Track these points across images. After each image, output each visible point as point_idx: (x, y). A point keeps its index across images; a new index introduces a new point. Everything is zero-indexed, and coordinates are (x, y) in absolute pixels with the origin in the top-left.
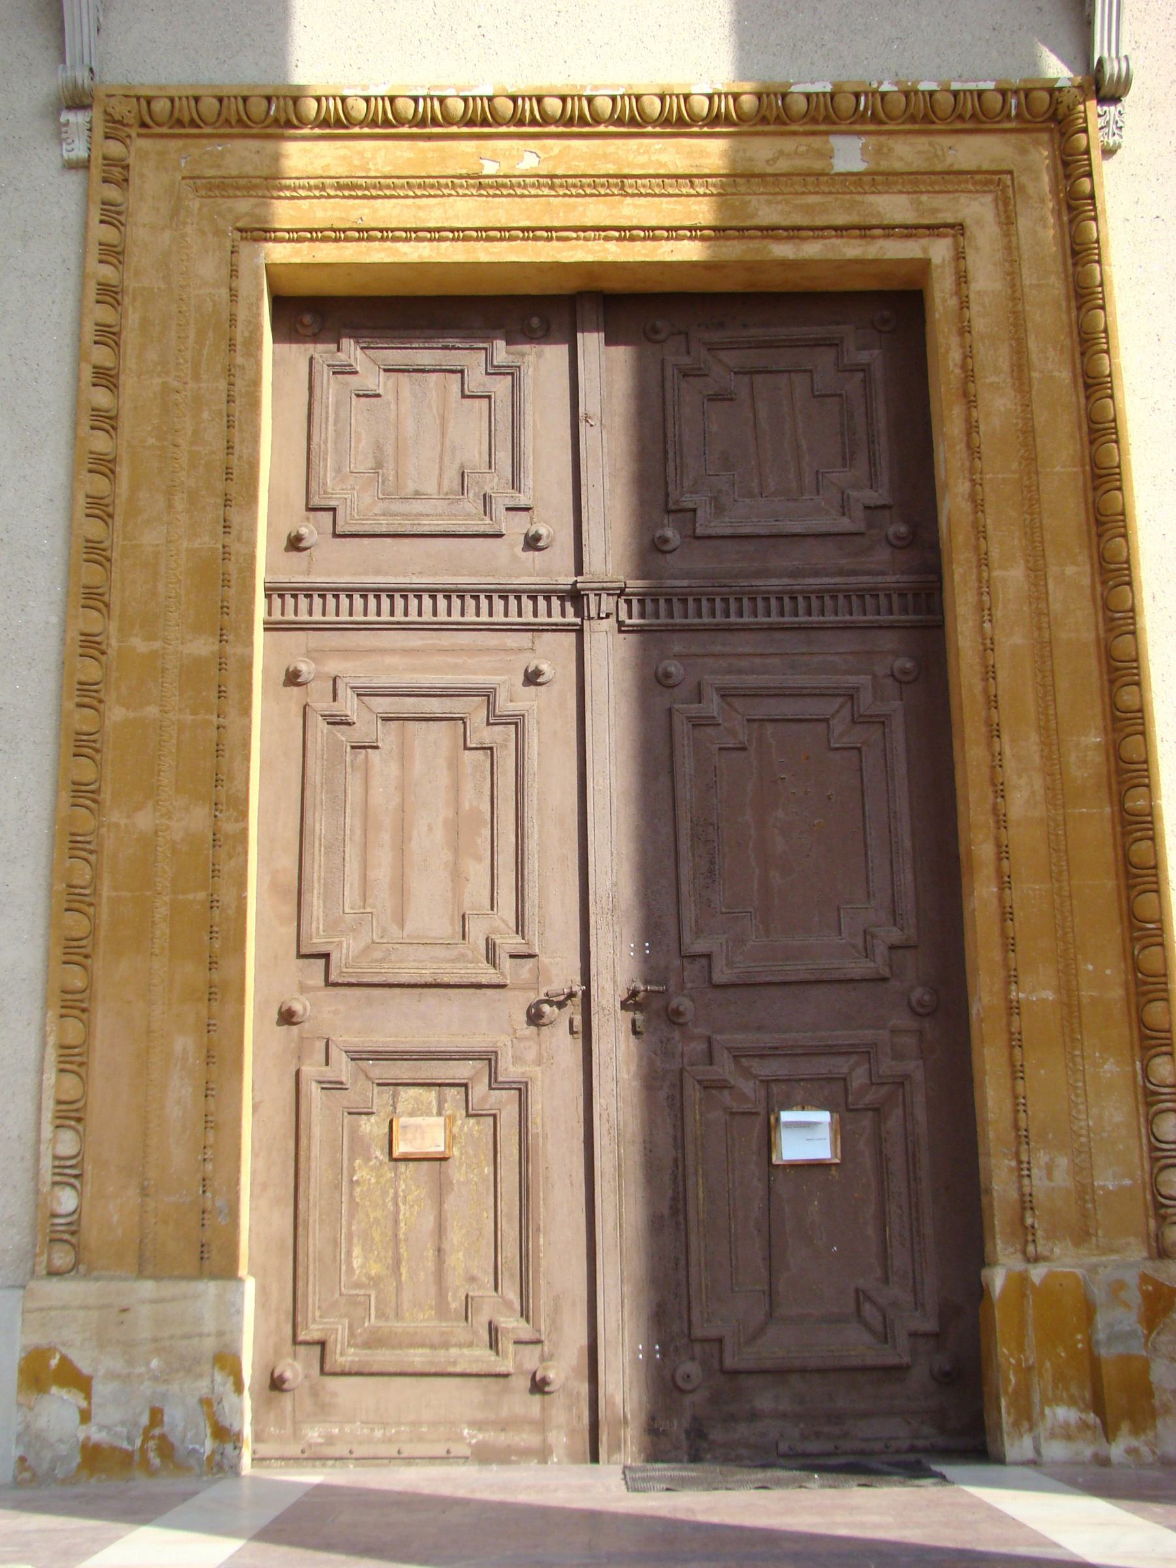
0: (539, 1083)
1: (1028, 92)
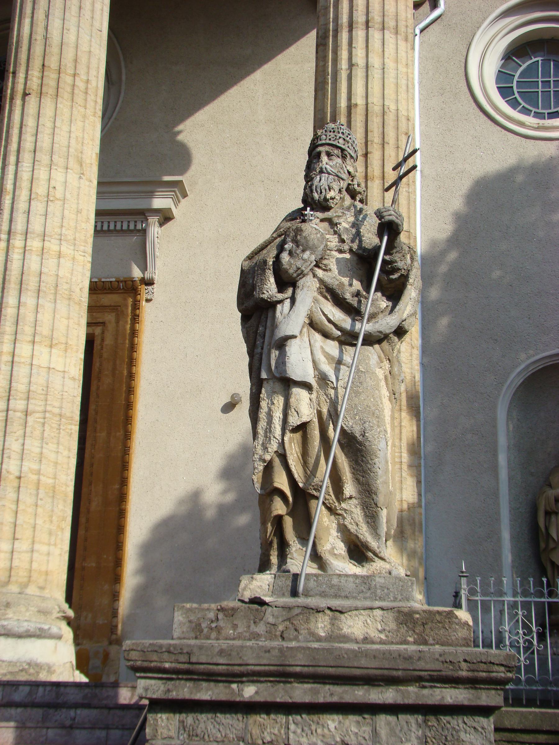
0: (409, 48)
1: (125, 282)
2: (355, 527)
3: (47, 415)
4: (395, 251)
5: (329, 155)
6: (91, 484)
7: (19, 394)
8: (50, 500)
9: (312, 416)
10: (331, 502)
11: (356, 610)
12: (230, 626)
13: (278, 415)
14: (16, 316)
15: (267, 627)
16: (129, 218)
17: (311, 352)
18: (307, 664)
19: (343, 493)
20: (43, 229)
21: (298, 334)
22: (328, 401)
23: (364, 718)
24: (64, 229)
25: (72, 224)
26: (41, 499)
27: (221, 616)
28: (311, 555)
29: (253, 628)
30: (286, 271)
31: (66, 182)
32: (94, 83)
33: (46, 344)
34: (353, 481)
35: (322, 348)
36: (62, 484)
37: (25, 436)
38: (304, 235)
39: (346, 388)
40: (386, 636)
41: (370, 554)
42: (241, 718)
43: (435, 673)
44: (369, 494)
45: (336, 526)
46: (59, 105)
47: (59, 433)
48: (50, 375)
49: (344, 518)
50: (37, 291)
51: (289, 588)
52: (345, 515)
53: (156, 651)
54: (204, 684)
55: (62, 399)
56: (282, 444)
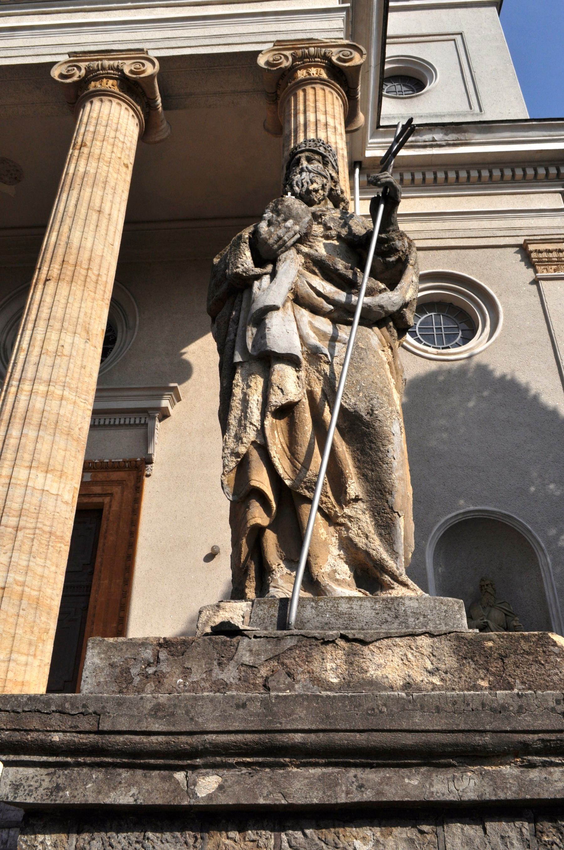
1: (130, 462)
2: (364, 541)
3: (37, 531)
4: (391, 228)
5: (309, 160)
6: (93, 623)
7: (12, 511)
8: (32, 611)
9: (300, 395)
10: (330, 506)
11: (387, 638)
12: (178, 672)
13: (255, 398)
14: (17, 445)
15: (240, 672)
16: (135, 415)
17: (298, 328)
18: (314, 727)
19: (346, 493)
20: (49, 377)
21: (281, 306)
22: (321, 378)
23: (422, 832)
24: (68, 378)
25: (76, 376)
26: (23, 610)
27: (163, 655)
28: (303, 582)
29: (218, 674)
30: (265, 241)
31: (73, 343)
32: (104, 278)
33: (42, 470)
34: (359, 478)
35: (310, 323)
36: (48, 597)
37: (13, 550)
38: (286, 204)
39: (343, 365)
40: (442, 680)
41: (387, 578)
42: (191, 841)
43: (553, 737)
44: (382, 494)
45: (337, 541)
46: (72, 288)
47: (48, 549)
48: (44, 496)
49: (348, 529)
50: (38, 426)
51: (275, 620)
52: (349, 524)
53: (39, 711)
54: (125, 774)
55: (54, 518)
56: (262, 432)
